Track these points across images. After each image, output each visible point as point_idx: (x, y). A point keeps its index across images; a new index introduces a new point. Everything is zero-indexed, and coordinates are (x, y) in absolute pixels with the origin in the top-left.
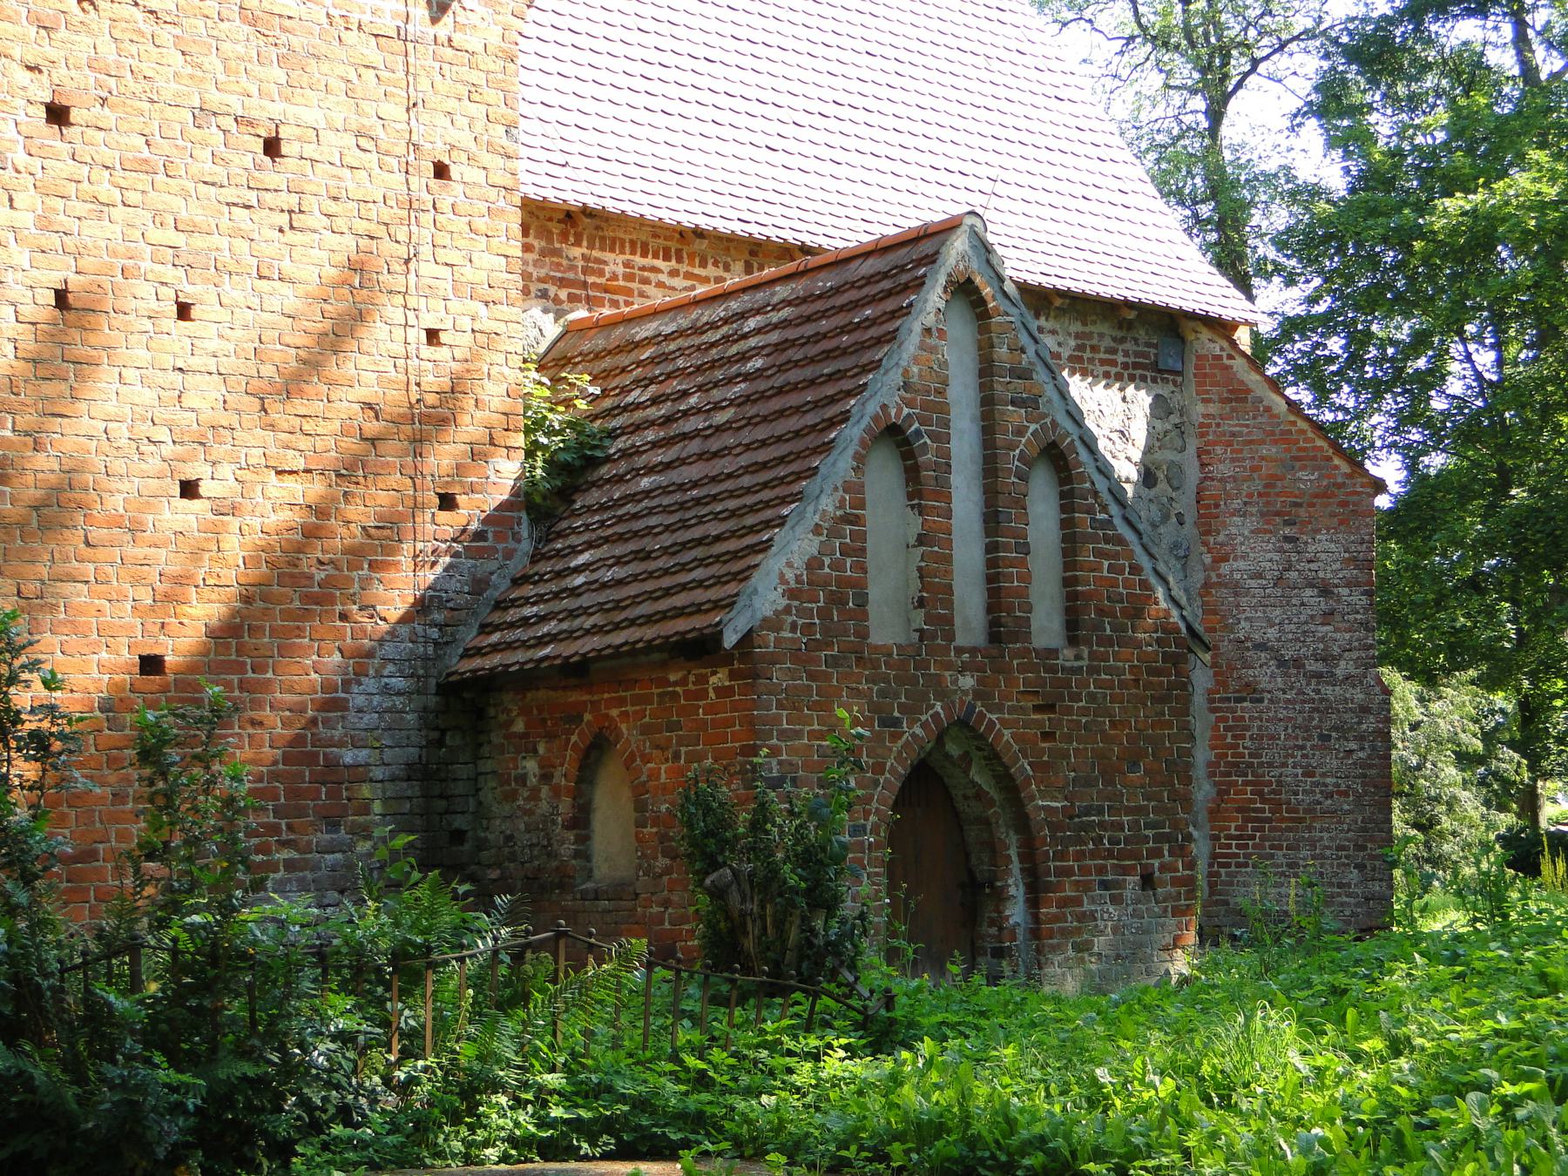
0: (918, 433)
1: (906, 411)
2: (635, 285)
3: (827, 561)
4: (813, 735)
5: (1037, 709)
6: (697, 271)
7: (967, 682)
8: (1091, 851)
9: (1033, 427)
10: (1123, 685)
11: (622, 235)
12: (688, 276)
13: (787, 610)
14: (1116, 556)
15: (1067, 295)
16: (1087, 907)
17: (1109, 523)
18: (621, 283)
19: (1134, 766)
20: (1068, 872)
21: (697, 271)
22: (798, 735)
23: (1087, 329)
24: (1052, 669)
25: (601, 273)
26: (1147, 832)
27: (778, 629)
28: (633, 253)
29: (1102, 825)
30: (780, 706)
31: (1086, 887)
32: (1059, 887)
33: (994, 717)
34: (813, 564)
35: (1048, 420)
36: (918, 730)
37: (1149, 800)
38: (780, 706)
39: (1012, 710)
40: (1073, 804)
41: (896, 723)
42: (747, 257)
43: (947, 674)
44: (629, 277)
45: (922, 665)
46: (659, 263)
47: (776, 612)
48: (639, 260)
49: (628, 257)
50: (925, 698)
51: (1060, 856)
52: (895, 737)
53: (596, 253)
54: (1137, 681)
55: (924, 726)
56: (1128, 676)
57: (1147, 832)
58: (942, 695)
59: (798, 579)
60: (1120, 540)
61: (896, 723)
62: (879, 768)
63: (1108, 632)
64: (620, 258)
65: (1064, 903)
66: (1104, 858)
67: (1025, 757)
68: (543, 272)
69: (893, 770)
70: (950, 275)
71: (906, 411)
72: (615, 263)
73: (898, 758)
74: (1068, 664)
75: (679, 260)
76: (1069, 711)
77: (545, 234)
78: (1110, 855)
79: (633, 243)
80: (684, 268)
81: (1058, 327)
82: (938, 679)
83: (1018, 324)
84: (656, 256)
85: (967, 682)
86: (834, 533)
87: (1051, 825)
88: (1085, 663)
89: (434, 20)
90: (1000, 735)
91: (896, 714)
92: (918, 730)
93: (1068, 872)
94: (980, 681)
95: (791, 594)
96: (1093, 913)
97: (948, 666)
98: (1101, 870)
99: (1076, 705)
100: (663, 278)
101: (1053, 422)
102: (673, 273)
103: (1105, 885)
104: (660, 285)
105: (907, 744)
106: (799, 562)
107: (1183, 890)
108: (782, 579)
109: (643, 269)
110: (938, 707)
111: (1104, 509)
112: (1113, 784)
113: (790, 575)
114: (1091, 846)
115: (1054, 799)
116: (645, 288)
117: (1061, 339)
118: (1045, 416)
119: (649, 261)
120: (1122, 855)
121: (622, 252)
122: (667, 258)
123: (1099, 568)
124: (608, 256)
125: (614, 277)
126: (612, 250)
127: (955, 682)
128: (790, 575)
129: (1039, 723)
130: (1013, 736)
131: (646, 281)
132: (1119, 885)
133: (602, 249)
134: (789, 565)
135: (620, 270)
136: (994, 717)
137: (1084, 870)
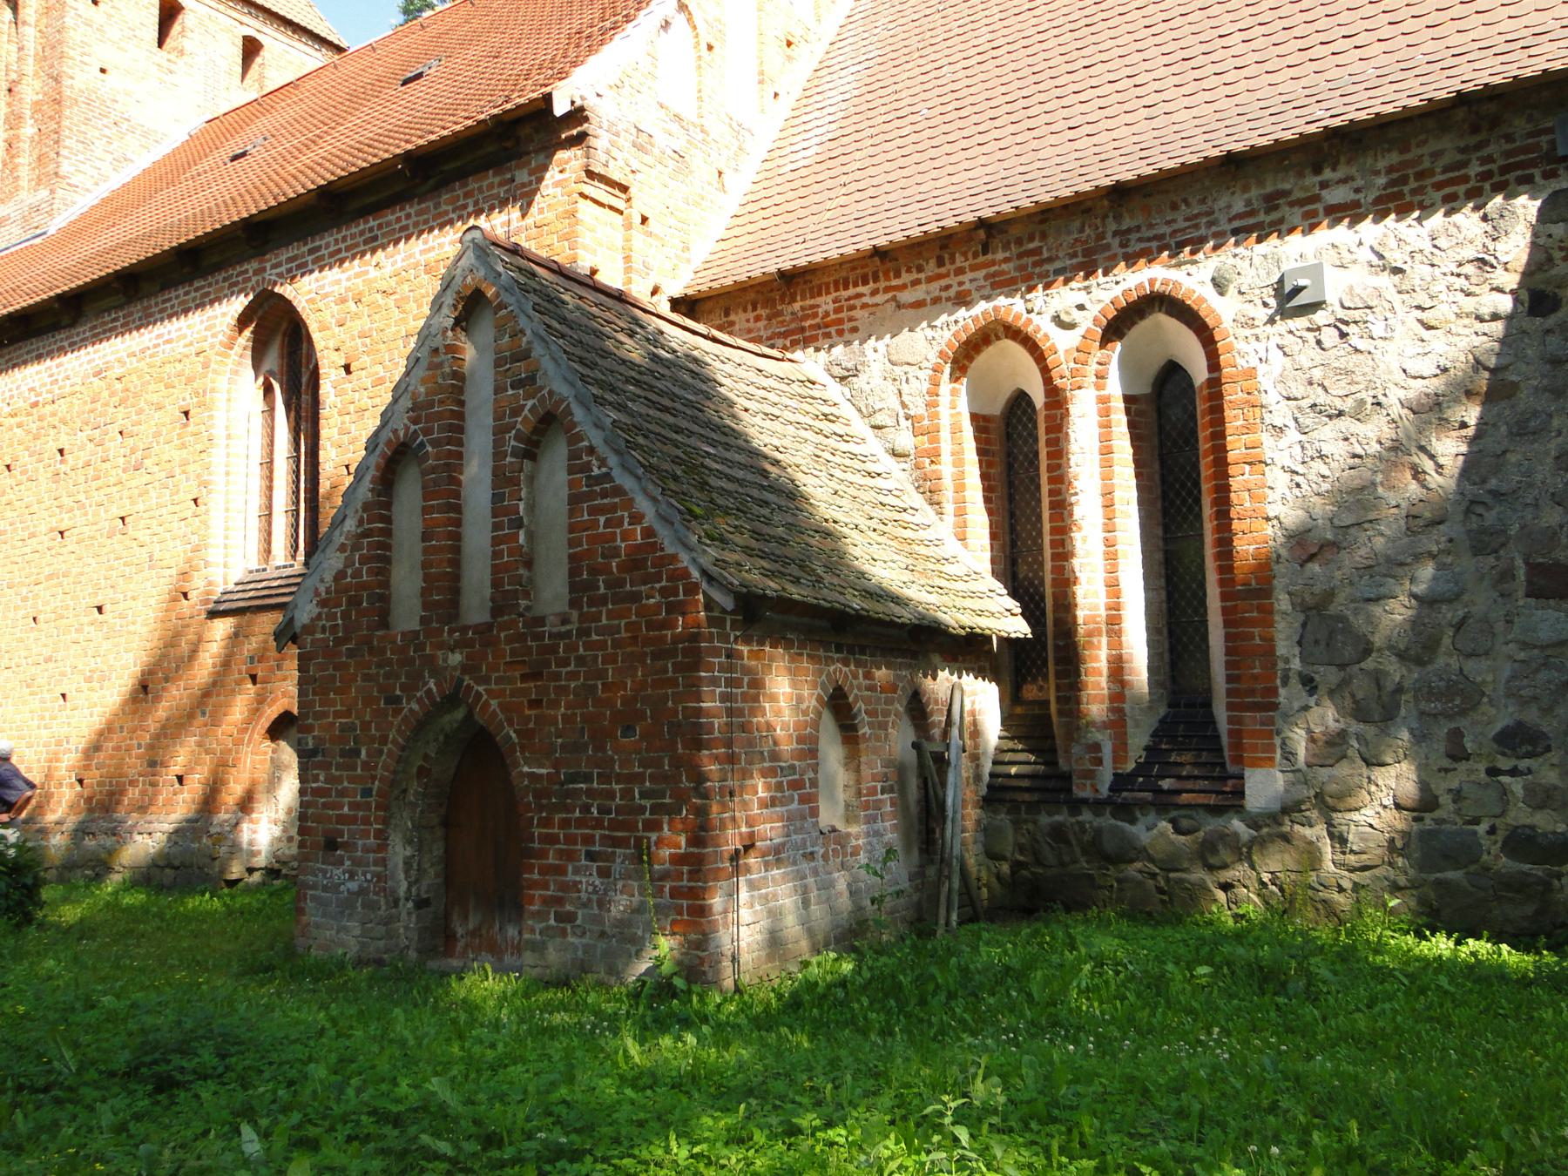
0: (422, 445)
1: (413, 427)
2: (843, 315)
3: (349, 571)
4: (337, 715)
5: (525, 678)
6: (894, 283)
7: (456, 658)
8: (577, 819)
9: (530, 403)
10: (616, 644)
11: (826, 280)
12: (887, 290)
13: (319, 617)
14: (613, 508)
15: (1331, 134)
16: (570, 877)
17: (607, 477)
18: (833, 317)
19: (628, 730)
20: (552, 839)
21: (894, 283)
22: (324, 715)
23: (1408, 156)
24: (540, 637)
25: (815, 315)
26: (643, 802)
27: (313, 633)
28: (837, 290)
29: (590, 793)
30: (315, 693)
31: (570, 856)
32: (542, 854)
33: (481, 689)
34: (340, 575)
35: (545, 392)
36: (415, 706)
37: (646, 767)
38: (315, 693)
39: (499, 681)
40: (558, 773)
41: (398, 700)
42: (938, 252)
43: (439, 653)
44: (838, 310)
45: (420, 647)
46: (860, 289)
47: (312, 620)
48: (845, 294)
49: (834, 295)
50: (420, 676)
51: (546, 823)
52: (397, 712)
53: (809, 302)
54: (635, 638)
55: (419, 701)
56: (624, 635)
57: (643, 802)
58: (435, 672)
59: (328, 591)
60: (618, 491)
61: (398, 700)
62: (384, 740)
63: (602, 590)
64: (829, 298)
65: (545, 870)
66: (593, 828)
67: (511, 724)
68: (769, 333)
69: (394, 742)
70: (458, 293)
71: (413, 427)
72: (826, 303)
73: (399, 731)
74: (555, 630)
75: (876, 280)
76: (557, 677)
77: (770, 303)
78: (598, 824)
79: (836, 283)
80: (882, 284)
81: (1353, 171)
82: (433, 658)
83: (517, 311)
84: (856, 285)
85: (456, 658)
86: (356, 547)
87: (539, 795)
88: (573, 627)
89: (523, 216)
90: (487, 704)
91: (398, 692)
92: (415, 706)
93: (552, 839)
94: (469, 657)
95: (323, 603)
96: (576, 883)
97: (441, 646)
98: (588, 840)
99: (564, 670)
100: (866, 300)
101: (551, 393)
102: (874, 293)
103: (591, 856)
104: (864, 306)
105: (405, 719)
106: (328, 577)
107: (685, 869)
108: (317, 593)
109: (849, 299)
110: (432, 684)
111: (603, 462)
112: (603, 749)
113: (322, 589)
114: (577, 814)
115: (541, 766)
116: (852, 313)
117: (1359, 183)
118: (542, 388)
119: (852, 291)
120: (615, 825)
121: (828, 293)
122: (865, 283)
123: (595, 524)
124: (818, 300)
125: (827, 314)
126: (820, 295)
127: (445, 660)
128: (322, 589)
129: (525, 692)
130: (500, 705)
131: (852, 308)
132: (610, 858)
133: (812, 297)
134: (322, 580)
135: (831, 307)
136: (481, 689)
137: (570, 839)
